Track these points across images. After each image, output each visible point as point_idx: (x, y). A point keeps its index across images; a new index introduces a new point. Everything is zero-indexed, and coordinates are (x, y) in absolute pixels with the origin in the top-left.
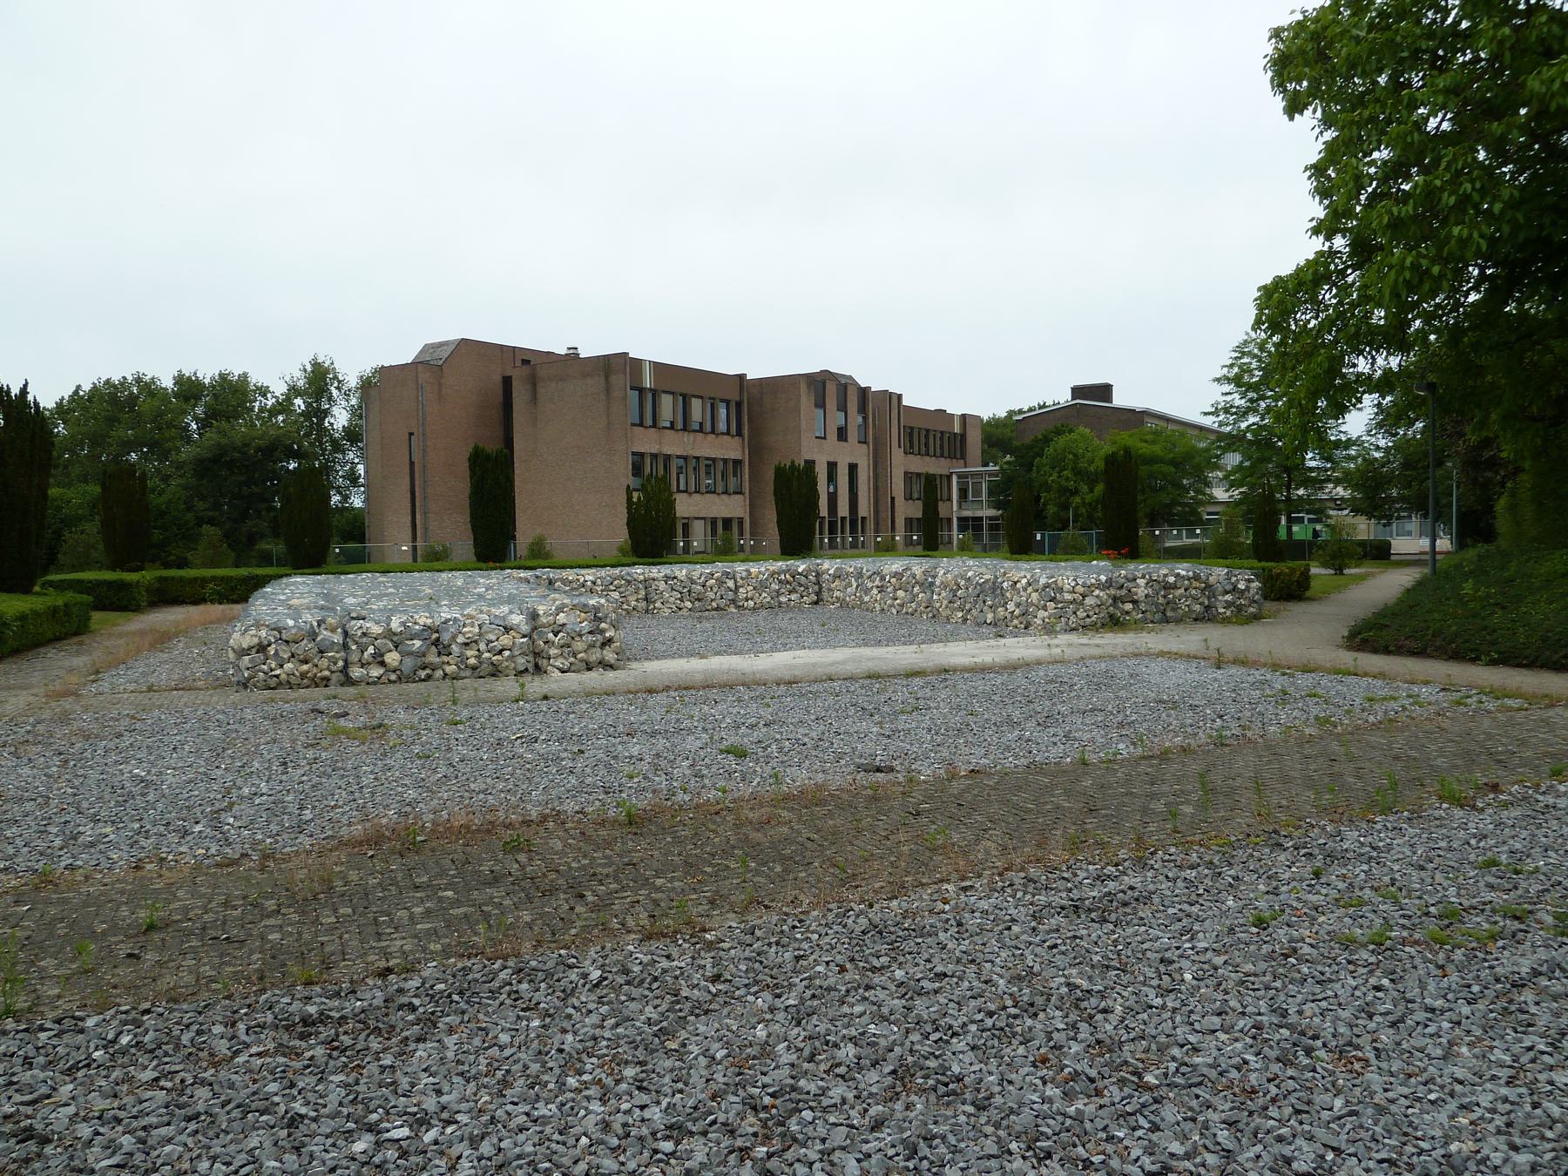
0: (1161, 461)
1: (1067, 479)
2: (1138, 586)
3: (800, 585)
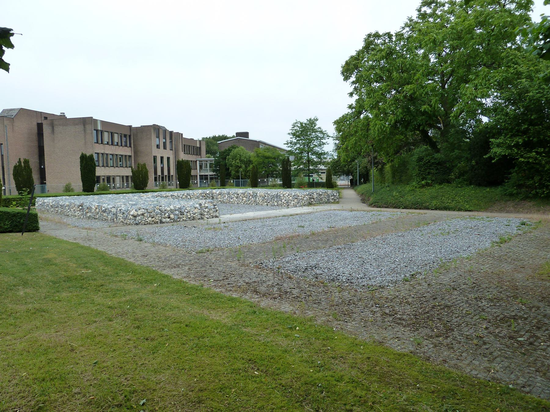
0: (271, 158)
1: (238, 163)
3: (208, 197)
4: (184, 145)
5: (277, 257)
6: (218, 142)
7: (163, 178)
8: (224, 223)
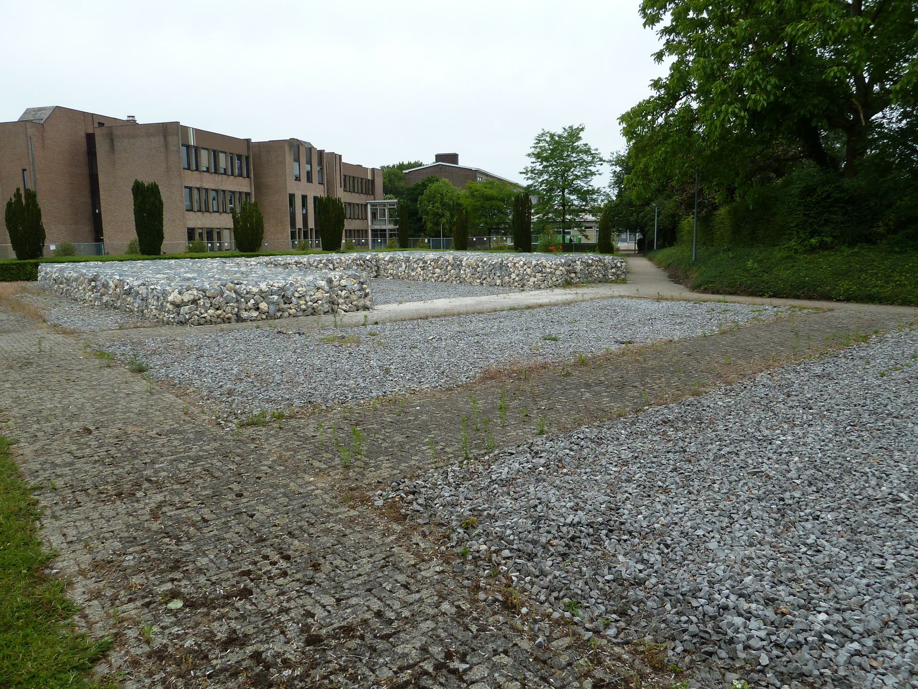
2: (577, 265)
3: (368, 267)
4: (345, 176)
5: (476, 451)
6: (404, 172)
7: (306, 233)
8: (376, 323)
